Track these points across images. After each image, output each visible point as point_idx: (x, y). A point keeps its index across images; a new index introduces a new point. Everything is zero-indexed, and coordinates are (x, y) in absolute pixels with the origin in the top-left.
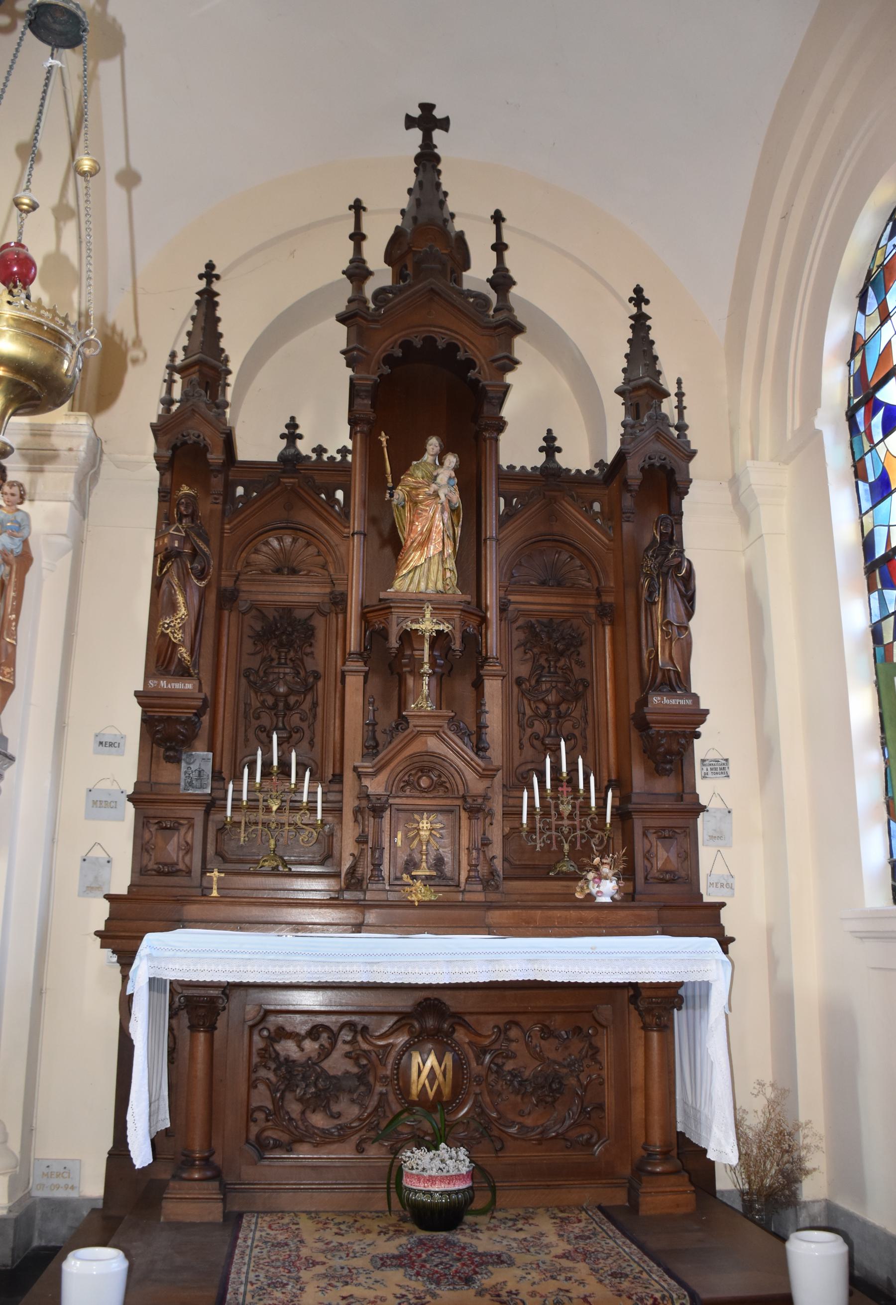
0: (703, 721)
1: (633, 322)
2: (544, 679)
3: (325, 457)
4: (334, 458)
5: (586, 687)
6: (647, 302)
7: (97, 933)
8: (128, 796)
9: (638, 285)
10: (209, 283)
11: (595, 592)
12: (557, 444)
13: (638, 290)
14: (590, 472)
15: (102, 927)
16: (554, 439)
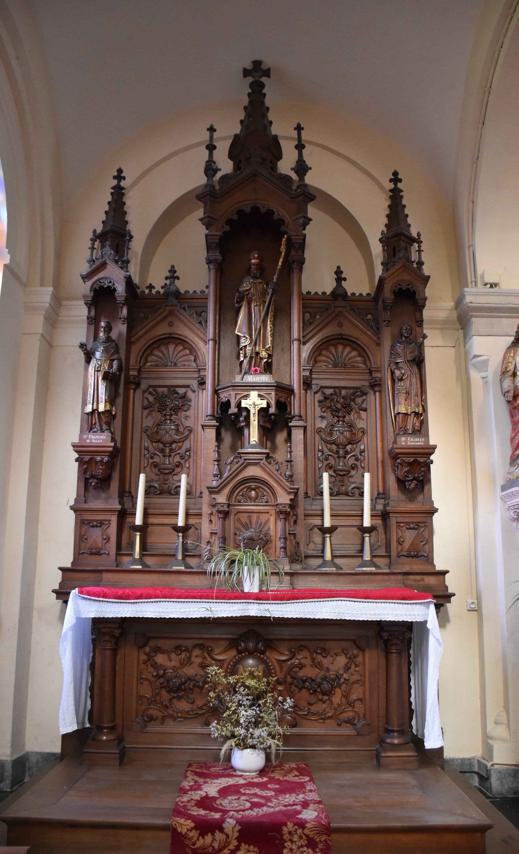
0: (433, 453)
1: (392, 194)
2: (336, 429)
3: (154, 292)
4: (160, 292)
5: (190, 431)
6: (400, 181)
7: (54, 591)
8: (70, 507)
9: (395, 171)
10: (396, 185)
11: (368, 371)
12: (343, 276)
13: (395, 174)
14: (368, 295)
15: (57, 587)
16: (342, 272)
